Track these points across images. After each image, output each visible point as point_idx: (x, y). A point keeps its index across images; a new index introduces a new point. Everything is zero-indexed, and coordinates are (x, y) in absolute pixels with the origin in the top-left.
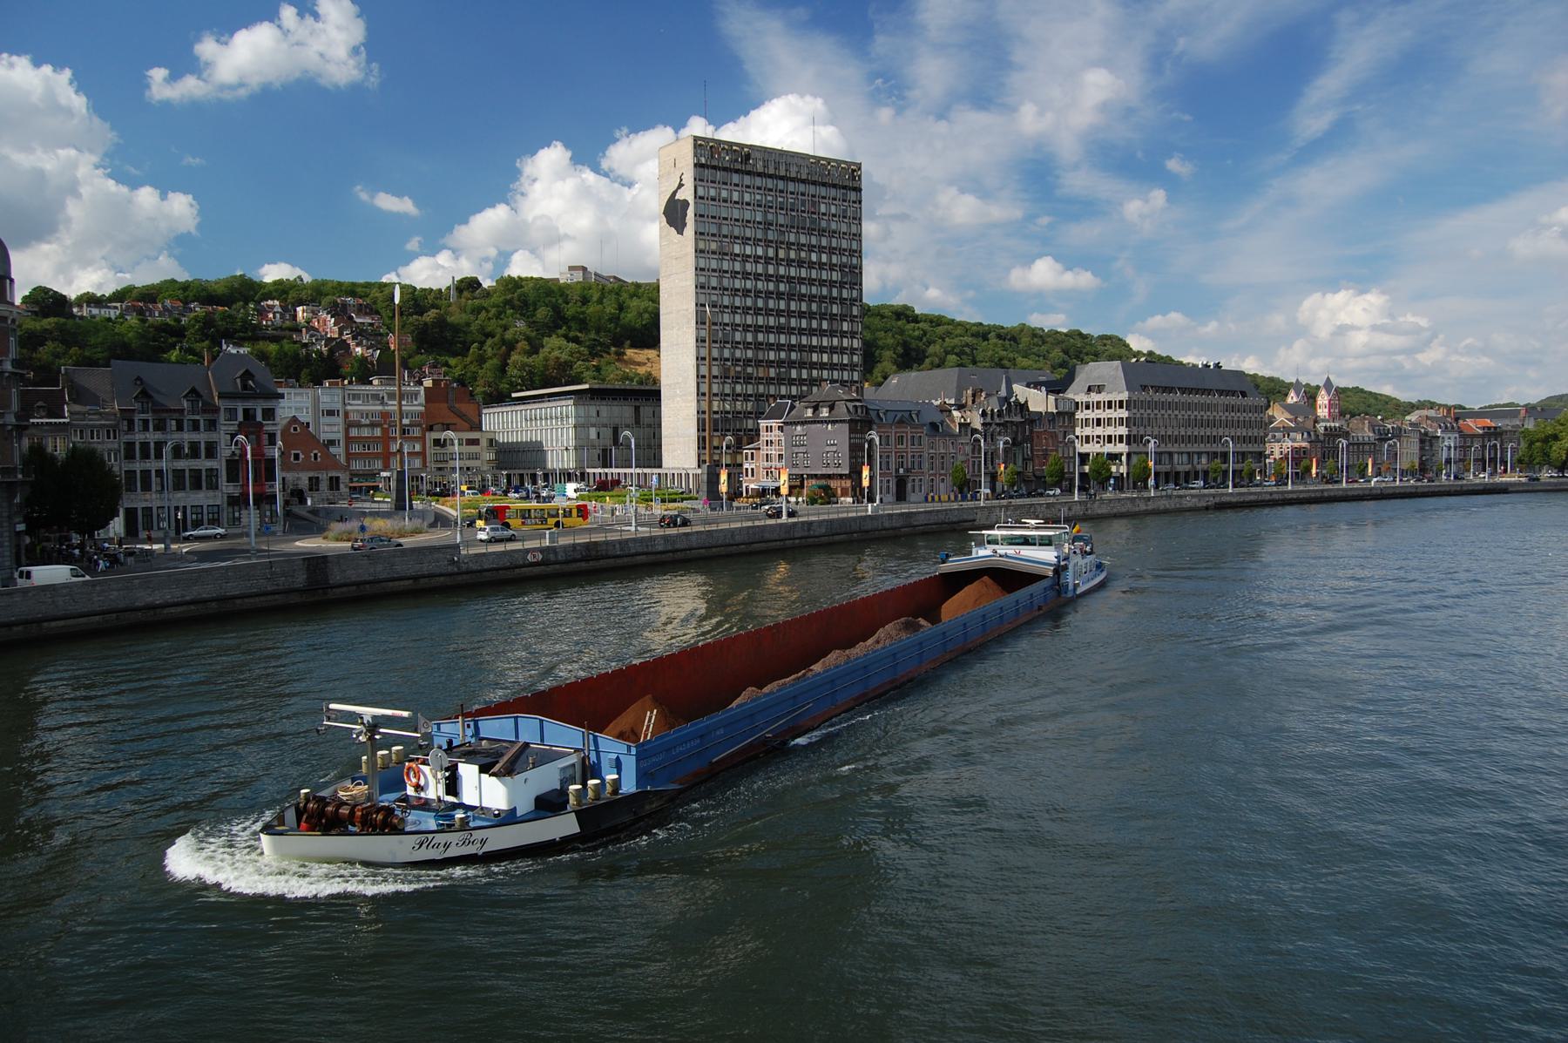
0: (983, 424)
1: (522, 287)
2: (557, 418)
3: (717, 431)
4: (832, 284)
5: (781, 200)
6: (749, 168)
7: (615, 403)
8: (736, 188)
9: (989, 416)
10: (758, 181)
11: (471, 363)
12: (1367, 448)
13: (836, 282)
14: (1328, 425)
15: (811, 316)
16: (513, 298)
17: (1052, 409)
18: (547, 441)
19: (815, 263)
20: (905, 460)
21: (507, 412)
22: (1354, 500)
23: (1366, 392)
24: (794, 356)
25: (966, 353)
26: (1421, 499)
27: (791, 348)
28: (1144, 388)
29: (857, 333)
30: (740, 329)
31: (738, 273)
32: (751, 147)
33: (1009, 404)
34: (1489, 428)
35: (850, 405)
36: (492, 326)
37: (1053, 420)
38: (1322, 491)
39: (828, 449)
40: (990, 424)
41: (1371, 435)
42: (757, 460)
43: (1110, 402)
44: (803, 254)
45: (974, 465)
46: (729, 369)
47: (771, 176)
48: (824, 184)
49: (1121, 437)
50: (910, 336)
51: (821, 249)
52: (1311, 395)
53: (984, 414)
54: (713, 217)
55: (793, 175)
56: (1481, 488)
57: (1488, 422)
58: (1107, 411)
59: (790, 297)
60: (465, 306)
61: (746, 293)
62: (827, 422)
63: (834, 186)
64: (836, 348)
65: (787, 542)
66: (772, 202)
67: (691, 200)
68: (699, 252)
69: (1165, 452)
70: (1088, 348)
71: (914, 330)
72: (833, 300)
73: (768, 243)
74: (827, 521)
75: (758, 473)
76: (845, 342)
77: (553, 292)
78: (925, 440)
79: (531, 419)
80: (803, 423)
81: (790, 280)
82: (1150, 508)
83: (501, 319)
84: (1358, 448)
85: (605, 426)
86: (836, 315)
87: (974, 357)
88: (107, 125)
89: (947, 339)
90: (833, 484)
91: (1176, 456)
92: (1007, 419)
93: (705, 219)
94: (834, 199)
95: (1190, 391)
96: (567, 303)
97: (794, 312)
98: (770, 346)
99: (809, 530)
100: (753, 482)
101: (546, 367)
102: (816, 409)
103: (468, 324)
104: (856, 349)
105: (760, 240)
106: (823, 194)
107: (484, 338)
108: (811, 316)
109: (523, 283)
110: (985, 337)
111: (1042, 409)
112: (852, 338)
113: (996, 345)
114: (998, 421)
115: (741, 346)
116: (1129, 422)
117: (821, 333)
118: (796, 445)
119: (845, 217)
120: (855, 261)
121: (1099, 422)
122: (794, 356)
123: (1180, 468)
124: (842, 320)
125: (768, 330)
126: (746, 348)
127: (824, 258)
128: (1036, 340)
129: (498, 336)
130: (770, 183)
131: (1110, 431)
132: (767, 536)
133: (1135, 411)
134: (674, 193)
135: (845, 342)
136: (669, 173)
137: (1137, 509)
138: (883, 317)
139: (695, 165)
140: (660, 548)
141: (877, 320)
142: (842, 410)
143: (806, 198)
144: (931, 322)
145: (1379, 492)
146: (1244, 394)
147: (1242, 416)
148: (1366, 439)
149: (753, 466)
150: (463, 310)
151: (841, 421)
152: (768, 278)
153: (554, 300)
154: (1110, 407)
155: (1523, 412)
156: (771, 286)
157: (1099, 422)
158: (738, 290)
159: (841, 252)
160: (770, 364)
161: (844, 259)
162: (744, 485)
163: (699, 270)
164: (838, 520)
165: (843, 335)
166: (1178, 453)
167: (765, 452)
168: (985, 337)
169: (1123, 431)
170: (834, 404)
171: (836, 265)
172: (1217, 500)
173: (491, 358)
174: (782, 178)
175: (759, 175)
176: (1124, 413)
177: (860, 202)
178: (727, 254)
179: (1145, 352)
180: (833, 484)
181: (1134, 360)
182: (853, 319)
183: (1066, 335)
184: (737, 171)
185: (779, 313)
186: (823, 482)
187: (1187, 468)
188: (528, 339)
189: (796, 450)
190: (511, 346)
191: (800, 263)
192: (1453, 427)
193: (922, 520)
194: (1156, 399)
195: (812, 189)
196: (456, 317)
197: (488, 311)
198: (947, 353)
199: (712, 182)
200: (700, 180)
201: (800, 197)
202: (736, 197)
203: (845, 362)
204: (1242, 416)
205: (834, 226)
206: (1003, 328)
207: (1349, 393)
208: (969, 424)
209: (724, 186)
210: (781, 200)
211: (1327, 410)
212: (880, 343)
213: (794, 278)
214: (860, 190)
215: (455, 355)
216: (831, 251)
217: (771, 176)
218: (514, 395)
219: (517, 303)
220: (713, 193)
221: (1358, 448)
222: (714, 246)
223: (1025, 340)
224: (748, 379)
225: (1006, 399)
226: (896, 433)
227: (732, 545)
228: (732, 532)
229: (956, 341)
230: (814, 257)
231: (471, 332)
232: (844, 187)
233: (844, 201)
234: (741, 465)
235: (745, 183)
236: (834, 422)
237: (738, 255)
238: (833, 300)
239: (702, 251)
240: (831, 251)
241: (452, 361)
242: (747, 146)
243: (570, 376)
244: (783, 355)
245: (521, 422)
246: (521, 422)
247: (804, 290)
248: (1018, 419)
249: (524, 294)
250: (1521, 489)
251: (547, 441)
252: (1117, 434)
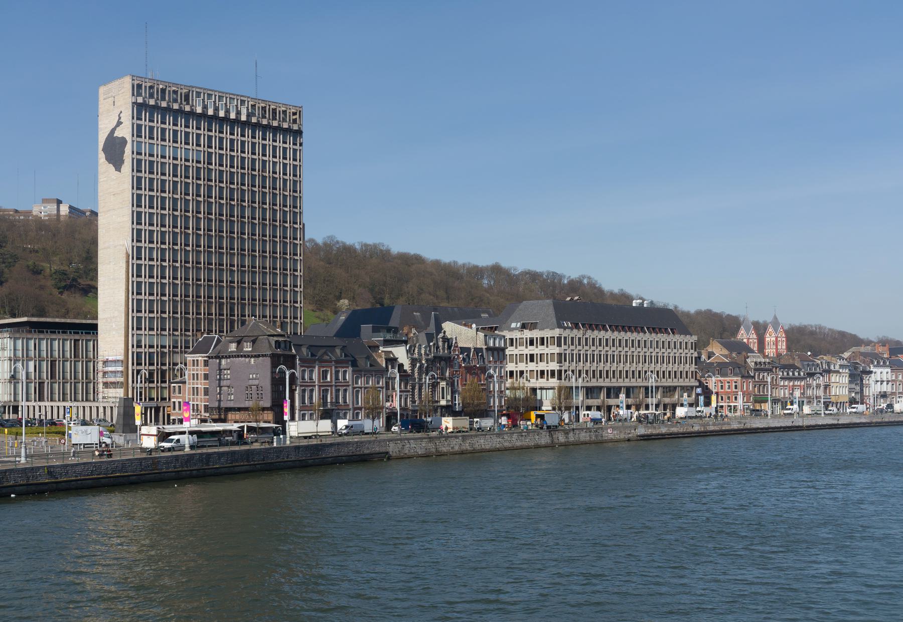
43: (542, 339)
49: (553, 372)
52: (760, 329)
58: (540, 347)
91: (538, 391)
131: (542, 366)
133: (566, 347)
134: (113, 131)
151: (263, 356)
154: (542, 344)
166: (541, 389)
167: (192, 386)
169: (554, 366)
236: (255, 356)
252: (550, 369)
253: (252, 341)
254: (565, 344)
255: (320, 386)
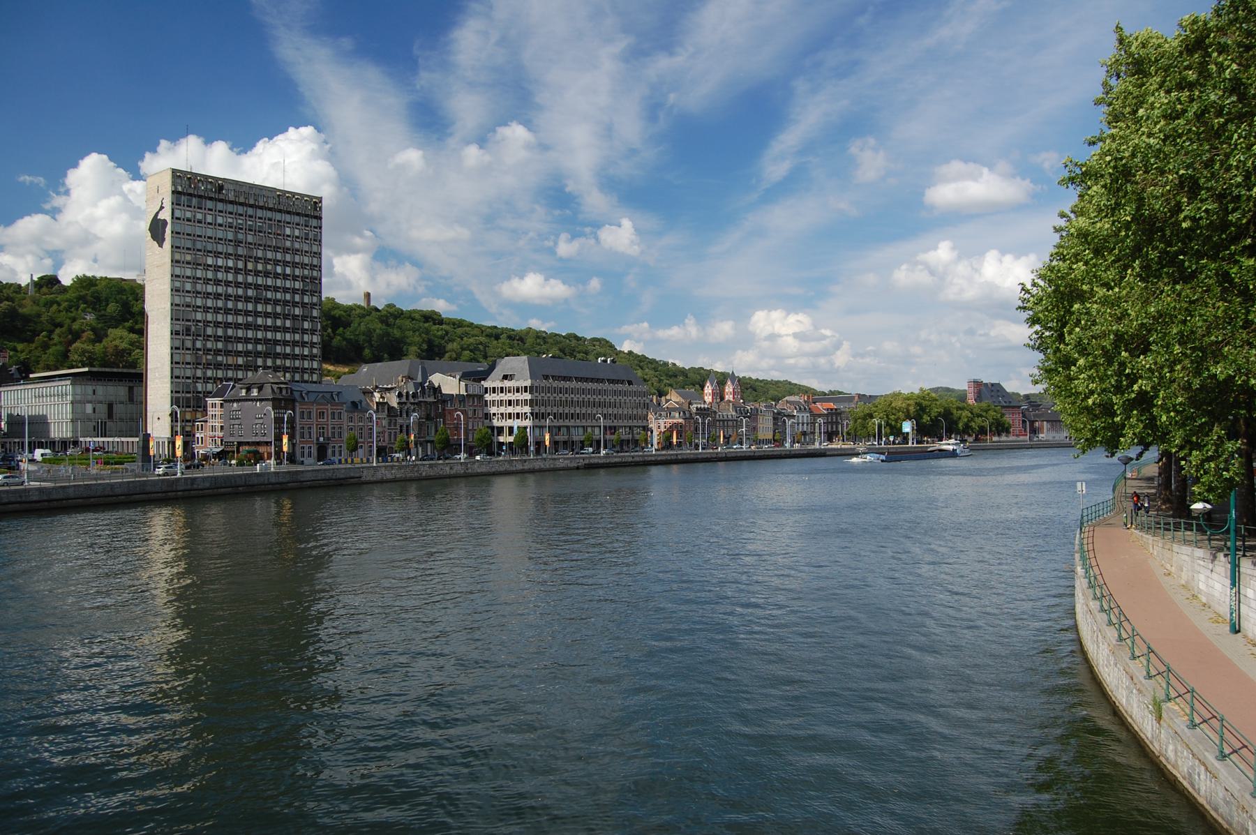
0: (398, 403)
1: (96, 285)
2: (58, 395)
3: (190, 407)
4: (295, 291)
5: (251, 223)
6: (221, 197)
7: (110, 383)
8: (210, 212)
9: (405, 397)
10: (230, 208)
11: (36, 348)
12: (730, 423)
13: (298, 290)
14: (699, 406)
15: (275, 316)
16: (87, 294)
17: (463, 392)
18: (50, 414)
19: (280, 274)
20: (325, 431)
21: (62, 386)
22: (735, 460)
23: (793, 384)
24: (260, 348)
25: (479, 350)
26: (779, 460)
27: (257, 341)
28: (546, 377)
29: (316, 331)
30: (212, 325)
31: (211, 280)
32: (224, 180)
33: (423, 388)
34: (832, 409)
35: (275, 386)
36: (62, 317)
37: (464, 400)
38: (677, 455)
39: (257, 421)
40: (405, 403)
41: (734, 413)
42: (206, 431)
44: (269, 267)
45: (390, 435)
46: (201, 357)
47: (241, 204)
48: (289, 213)
50: (434, 335)
51: (285, 264)
53: (400, 395)
54: (188, 235)
55: (261, 204)
56: (805, 452)
57: (832, 405)
58: (516, 394)
59: (257, 300)
60: (39, 301)
61: (217, 296)
62: (257, 400)
63: (298, 214)
64: (298, 342)
65: (170, 494)
66: (242, 224)
67: (169, 219)
68: (175, 262)
69: (563, 426)
70: (580, 348)
71: (438, 331)
72: (295, 304)
73: (237, 257)
74: (212, 477)
75: (206, 441)
76: (306, 338)
77: (125, 290)
78: (345, 416)
79: (39, 396)
80: (238, 401)
81: (257, 287)
82: (526, 467)
83: (71, 312)
84: (724, 424)
85: (101, 402)
86: (298, 316)
87: (486, 353)
88: (291, 130)
89: (465, 338)
90: (262, 449)
91: (635, 429)
92: (421, 399)
93: (181, 236)
94: (298, 224)
95: (586, 380)
96: (137, 301)
97: (261, 312)
98: (238, 340)
99: (192, 484)
100: (201, 448)
101: (105, 353)
102: (249, 390)
103: (39, 316)
104: (316, 343)
105: (231, 255)
106: (288, 220)
107: (53, 328)
108: (275, 316)
109: (98, 282)
110: (497, 337)
111: (455, 392)
112: (312, 334)
113: (504, 344)
114: (412, 401)
115: (212, 339)
116: (532, 403)
117: (285, 330)
118: (233, 419)
119: (307, 239)
120: (315, 274)
121: (510, 403)
122: (260, 348)
123: (575, 438)
124: (303, 320)
125: (237, 326)
126: (217, 341)
127: (288, 271)
128: (538, 341)
129: (66, 326)
130: (241, 210)
131: (518, 409)
132: (148, 489)
133: (537, 394)
134: (157, 213)
135: (306, 338)
136: (153, 197)
137: (514, 469)
138: (413, 319)
139: (173, 192)
140: (35, 498)
141: (407, 323)
142: (267, 393)
143: (273, 222)
144: (454, 324)
145: (724, 455)
146: (630, 383)
147: (569, 397)
148: (726, 417)
149: (202, 435)
150: (36, 302)
152: (238, 285)
153: (124, 297)
155: (856, 398)
156: (240, 292)
157: (510, 403)
158: (210, 294)
159: (303, 266)
160: (238, 354)
161: (306, 272)
162: (196, 451)
163: (174, 277)
164: (222, 476)
165: (304, 331)
168: (497, 337)
170: (262, 386)
171: (298, 277)
172: (587, 461)
173: (55, 345)
174: (251, 206)
175: (231, 202)
176: (528, 396)
177: (320, 228)
178: (200, 265)
179: (626, 351)
180: (262, 449)
181: (544, 356)
182: (313, 319)
183: (564, 337)
184: (211, 199)
185: (247, 313)
186: (253, 448)
187: (582, 438)
188: (93, 329)
189: (233, 422)
190: (77, 336)
191: (267, 274)
192: (805, 409)
193: (308, 477)
194: (555, 385)
195: (278, 216)
196: (27, 309)
197: (59, 304)
198: (463, 349)
199: (188, 206)
200: (177, 204)
201: (267, 222)
202: (209, 219)
203: (306, 353)
204: (569, 397)
205: (297, 246)
206: (513, 330)
207: (780, 385)
208: (387, 403)
209: (199, 210)
210: (251, 223)
211: (731, 396)
212: (408, 341)
213: (261, 286)
214: (321, 218)
215: (22, 341)
216: (294, 265)
217: (241, 204)
218: (31, 376)
219: (89, 298)
220: (189, 215)
221: (724, 424)
222: (188, 258)
223: (529, 341)
224: (218, 366)
225: (422, 384)
226: (317, 409)
227: (112, 496)
228: (112, 486)
229: (471, 340)
230: (279, 270)
231: (41, 322)
232: (307, 216)
233: (307, 226)
234: (194, 435)
235: (218, 208)
236: (261, 400)
237: (210, 266)
238: (295, 304)
239: (178, 262)
240: (294, 265)
241: (20, 346)
242: (220, 179)
243: (127, 362)
244: (250, 347)
245: (32, 398)
246: (32, 398)
247: (269, 295)
248: (432, 399)
249: (97, 292)
250: (836, 453)
251: (50, 414)
253: (258, 388)
254: (536, 392)
255: (317, 425)
